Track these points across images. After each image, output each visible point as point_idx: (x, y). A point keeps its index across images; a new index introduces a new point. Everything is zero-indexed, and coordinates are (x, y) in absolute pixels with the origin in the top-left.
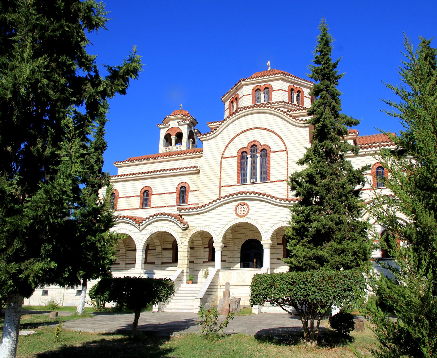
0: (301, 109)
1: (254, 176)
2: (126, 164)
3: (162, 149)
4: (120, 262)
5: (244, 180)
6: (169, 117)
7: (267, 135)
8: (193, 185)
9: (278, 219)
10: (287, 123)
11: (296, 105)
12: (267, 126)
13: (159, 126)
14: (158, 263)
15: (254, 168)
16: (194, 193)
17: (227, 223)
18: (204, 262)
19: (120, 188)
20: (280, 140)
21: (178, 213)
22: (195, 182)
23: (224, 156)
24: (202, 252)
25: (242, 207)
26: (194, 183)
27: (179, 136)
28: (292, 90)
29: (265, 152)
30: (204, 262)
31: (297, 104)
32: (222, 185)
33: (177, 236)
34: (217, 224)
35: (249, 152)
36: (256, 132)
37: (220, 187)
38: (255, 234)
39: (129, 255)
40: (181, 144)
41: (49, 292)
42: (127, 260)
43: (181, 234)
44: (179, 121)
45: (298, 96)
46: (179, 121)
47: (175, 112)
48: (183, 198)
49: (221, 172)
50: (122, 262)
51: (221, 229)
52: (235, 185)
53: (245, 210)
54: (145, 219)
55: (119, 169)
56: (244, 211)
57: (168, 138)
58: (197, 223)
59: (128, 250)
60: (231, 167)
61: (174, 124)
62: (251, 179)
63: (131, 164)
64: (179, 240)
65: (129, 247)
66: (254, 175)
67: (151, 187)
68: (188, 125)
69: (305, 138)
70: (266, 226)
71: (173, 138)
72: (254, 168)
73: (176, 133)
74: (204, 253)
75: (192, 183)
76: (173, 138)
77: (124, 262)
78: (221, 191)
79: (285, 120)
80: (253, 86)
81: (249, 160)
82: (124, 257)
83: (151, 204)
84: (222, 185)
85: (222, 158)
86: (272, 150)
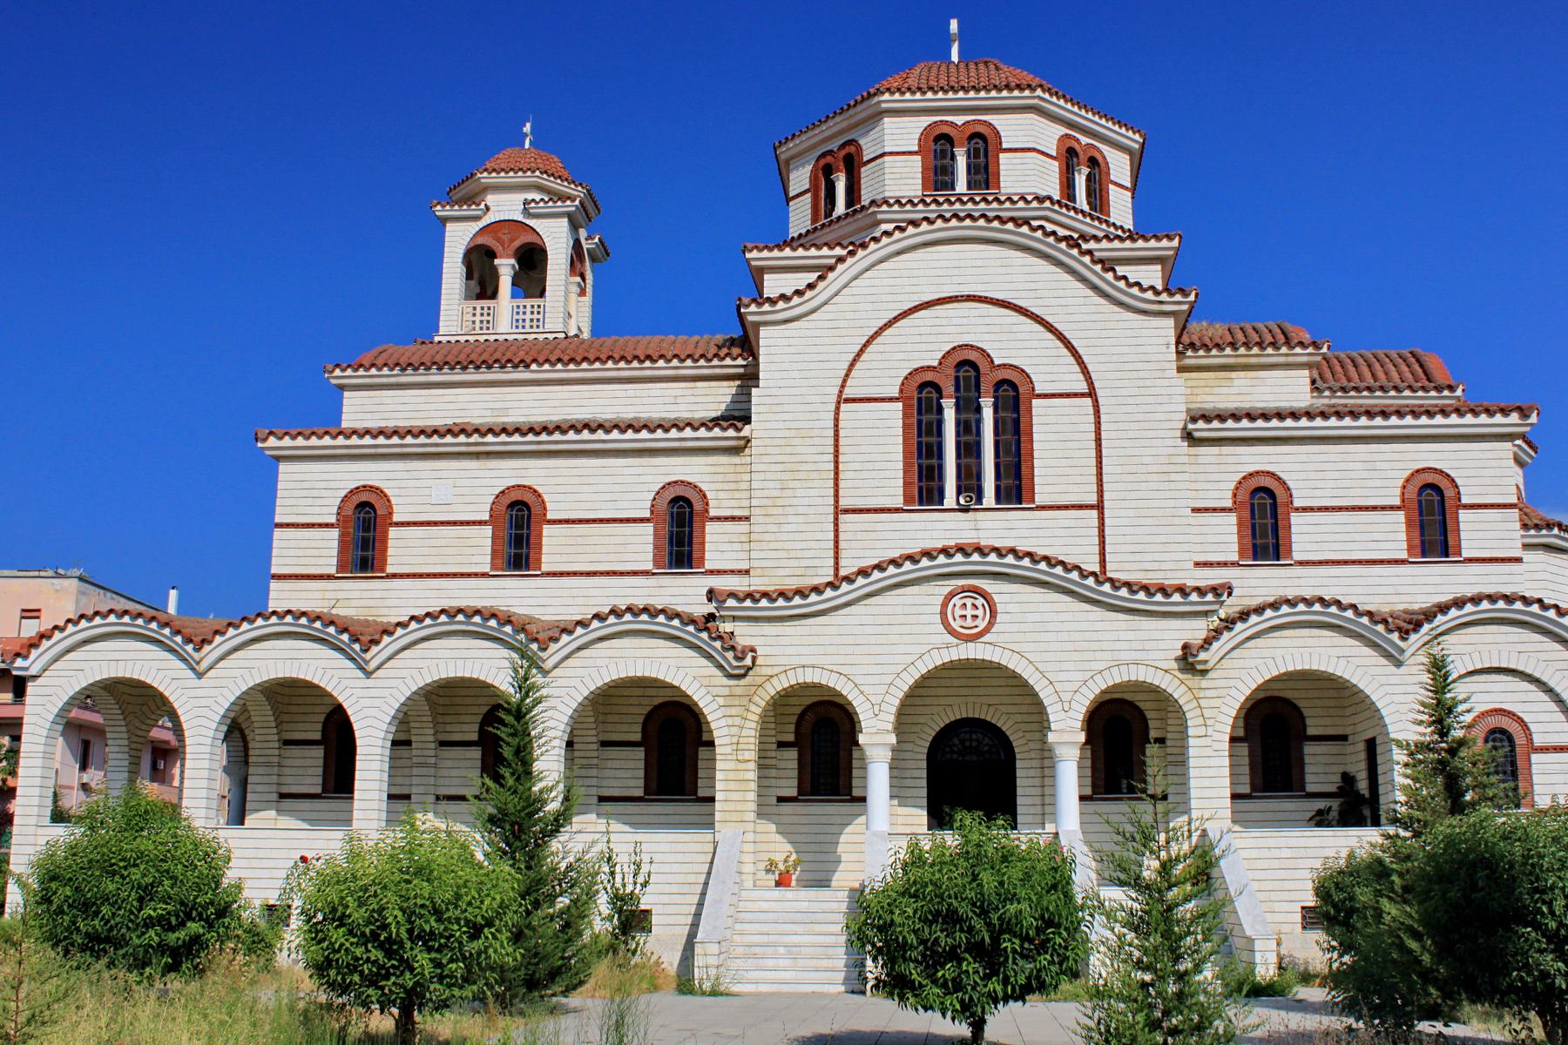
0: (1118, 237)
1: (970, 484)
2: (384, 380)
3: (455, 316)
4: (414, 790)
5: (930, 491)
6: (485, 178)
7: (1015, 328)
8: (722, 495)
9: (1108, 656)
10: (1089, 292)
11: (1082, 212)
12: (988, 287)
13: (440, 211)
14: (423, 798)
15: (969, 449)
16: (728, 526)
17: (909, 659)
18: (781, 799)
19: (393, 484)
20: (1065, 351)
21: (703, 608)
22: (733, 486)
23: (849, 392)
24: (773, 762)
25: (969, 602)
26: (726, 486)
27: (532, 260)
28: (1071, 152)
29: (1014, 396)
30: (781, 799)
31: (1086, 208)
32: (843, 503)
33: (709, 698)
34: (876, 661)
35: (948, 387)
36: (976, 312)
37: (838, 511)
38: (985, 700)
39: (449, 763)
40: (542, 294)
41: (655, 919)
42: (441, 781)
43: (726, 691)
44: (530, 196)
45: (1089, 178)
46: (530, 196)
47: (503, 157)
48: (680, 543)
49: (836, 455)
50: (421, 789)
51: (889, 679)
52: (897, 510)
53: (980, 612)
54: (570, 627)
55: (346, 394)
56: (975, 617)
57: (480, 264)
58: (793, 655)
59: (443, 744)
60: (881, 441)
61: (504, 206)
62: (959, 493)
63: (403, 379)
64: (719, 714)
65: (448, 728)
66: (969, 475)
67: (540, 490)
68: (569, 216)
69: (1161, 357)
70: (1062, 676)
71: (506, 267)
72: (969, 449)
73: (517, 244)
74: (782, 764)
75: (720, 486)
76: (506, 267)
77: (274, 788)
78: (842, 527)
79: (1083, 280)
80: (926, 121)
81: (950, 415)
82: (432, 771)
83: (544, 558)
84: (843, 503)
85: (841, 400)
86: (1039, 389)
